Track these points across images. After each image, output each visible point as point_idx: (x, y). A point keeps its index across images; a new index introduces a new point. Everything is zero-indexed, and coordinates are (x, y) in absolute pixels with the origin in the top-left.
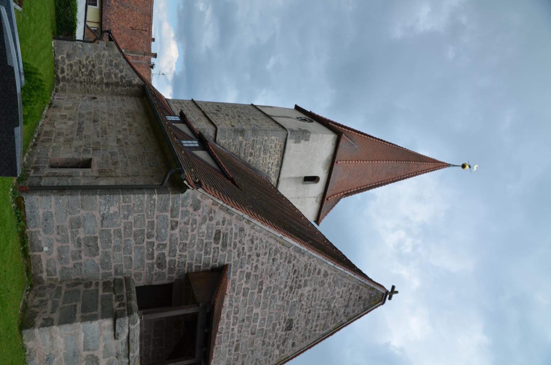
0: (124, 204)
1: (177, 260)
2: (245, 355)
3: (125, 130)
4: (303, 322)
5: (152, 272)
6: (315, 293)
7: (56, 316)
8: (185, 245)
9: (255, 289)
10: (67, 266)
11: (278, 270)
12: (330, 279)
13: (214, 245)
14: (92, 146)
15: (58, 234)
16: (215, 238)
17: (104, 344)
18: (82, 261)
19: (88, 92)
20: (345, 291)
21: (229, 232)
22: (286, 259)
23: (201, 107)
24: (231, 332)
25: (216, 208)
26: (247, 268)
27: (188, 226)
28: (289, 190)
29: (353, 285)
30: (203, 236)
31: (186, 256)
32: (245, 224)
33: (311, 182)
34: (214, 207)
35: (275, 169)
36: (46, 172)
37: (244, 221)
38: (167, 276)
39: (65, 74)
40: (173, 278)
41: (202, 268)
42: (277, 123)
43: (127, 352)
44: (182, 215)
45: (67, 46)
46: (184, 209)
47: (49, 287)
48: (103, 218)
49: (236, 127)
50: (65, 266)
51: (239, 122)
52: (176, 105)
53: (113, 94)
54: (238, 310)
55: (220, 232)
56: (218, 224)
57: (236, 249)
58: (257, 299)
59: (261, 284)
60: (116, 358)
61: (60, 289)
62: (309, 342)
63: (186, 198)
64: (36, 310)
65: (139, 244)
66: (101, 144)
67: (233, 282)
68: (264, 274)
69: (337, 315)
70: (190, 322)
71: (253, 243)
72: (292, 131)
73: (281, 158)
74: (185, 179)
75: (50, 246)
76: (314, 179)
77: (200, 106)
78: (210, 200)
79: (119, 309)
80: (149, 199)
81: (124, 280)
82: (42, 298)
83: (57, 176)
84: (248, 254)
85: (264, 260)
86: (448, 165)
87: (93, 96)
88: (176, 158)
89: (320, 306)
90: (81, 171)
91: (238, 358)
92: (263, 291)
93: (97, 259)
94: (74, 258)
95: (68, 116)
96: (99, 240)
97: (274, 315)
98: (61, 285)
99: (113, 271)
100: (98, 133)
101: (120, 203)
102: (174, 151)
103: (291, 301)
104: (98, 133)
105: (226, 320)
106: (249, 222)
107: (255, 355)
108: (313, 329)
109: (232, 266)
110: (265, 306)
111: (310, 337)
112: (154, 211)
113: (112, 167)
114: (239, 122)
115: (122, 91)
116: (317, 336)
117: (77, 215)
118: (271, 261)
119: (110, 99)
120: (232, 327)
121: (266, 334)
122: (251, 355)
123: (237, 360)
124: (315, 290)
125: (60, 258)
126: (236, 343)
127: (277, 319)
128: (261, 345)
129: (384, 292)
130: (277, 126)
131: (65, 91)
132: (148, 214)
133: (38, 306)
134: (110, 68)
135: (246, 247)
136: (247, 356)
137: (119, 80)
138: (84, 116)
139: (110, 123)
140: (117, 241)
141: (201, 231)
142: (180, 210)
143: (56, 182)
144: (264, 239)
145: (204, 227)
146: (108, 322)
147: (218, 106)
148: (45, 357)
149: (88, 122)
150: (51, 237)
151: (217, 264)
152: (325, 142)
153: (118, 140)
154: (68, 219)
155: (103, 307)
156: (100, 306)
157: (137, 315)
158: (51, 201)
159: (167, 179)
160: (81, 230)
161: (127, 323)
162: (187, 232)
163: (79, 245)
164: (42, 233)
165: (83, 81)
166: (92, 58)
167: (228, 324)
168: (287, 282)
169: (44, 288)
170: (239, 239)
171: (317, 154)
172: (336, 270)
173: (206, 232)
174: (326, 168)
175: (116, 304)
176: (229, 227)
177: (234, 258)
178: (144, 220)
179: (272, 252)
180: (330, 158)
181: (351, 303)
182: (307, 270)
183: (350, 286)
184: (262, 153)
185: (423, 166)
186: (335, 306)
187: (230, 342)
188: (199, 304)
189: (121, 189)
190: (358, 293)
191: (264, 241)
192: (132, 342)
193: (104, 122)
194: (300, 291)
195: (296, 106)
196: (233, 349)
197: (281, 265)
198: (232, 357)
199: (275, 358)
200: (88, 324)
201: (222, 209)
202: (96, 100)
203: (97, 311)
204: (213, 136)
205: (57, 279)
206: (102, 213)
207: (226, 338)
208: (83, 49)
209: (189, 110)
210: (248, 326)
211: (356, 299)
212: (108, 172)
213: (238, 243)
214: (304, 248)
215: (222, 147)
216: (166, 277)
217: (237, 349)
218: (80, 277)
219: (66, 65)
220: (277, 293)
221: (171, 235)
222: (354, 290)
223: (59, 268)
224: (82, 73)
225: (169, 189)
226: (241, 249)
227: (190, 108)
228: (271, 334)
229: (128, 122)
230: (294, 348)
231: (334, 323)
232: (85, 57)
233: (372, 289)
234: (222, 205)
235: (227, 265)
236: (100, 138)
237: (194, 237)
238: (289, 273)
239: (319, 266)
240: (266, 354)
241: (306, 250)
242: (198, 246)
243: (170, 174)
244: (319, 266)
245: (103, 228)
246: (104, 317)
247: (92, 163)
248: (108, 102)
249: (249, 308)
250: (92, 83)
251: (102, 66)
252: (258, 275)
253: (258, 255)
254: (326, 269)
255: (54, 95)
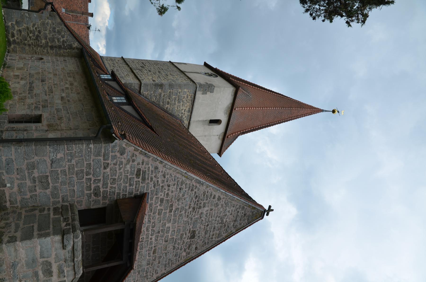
0: (68, 152)
1: (109, 190)
2: (161, 257)
3: (67, 88)
4: (203, 232)
5: (90, 200)
6: (211, 212)
7: (18, 234)
8: (114, 179)
9: (167, 210)
10: (26, 197)
11: (184, 196)
12: (222, 202)
13: (136, 179)
14: (41, 104)
15: (18, 174)
16: (136, 175)
17: (55, 253)
18: (37, 193)
19: (36, 53)
20: (233, 210)
21: (147, 169)
22: (189, 188)
23: (129, 64)
24: (150, 241)
25: (137, 153)
26: (161, 195)
27: (116, 166)
28: (198, 131)
29: (240, 206)
30: (128, 173)
31: (115, 188)
32: (159, 164)
33: (215, 124)
34: (136, 153)
35: (187, 114)
36: (5, 127)
37: (158, 162)
38: (101, 202)
39: (16, 38)
40: (106, 203)
41: (127, 196)
42: (189, 78)
43: (73, 258)
44: (112, 158)
45: (15, 14)
46: (113, 154)
47: (12, 213)
48: (52, 162)
49: (157, 82)
50: (24, 197)
51: (159, 77)
52: (109, 62)
53: (56, 55)
54: (155, 225)
55: (140, 170)
56: (138, 164)
57: (153, 182)
58: (169, 217)
59: (172, 206)
60: (64, 263)
61: (20, 214)
62: (207, 246)
63: (114, 146)
64: (3, 230)
65: (80, 179)
66: (49, 101)
67: (151, 205)
68: (173, 199)
69: (228, 227)
70: (119, 234)
71: (165, 177)
72: (201, 85)
73: (191, 106)
74: (114, 133)
75: (12, 183)
76: (217, 122)
77: (128, 63)
78: (132, 147)
79: (66, 228)
80: (87, 148)
81: (69, 206)
82: (7, 221)
83: (15, 130)
84: (161, 185)
85: (173, 189)
86: (322, 111)
87: (40, 56)
88: (107, 116)
89: (215, 221)
90: (33, 126)
91: (155, 259)
92: (173, 211)
93: (48, 191)
94: (31, 191)
95: (20, 76)
96: (49, 178)
97: (181, 228)
98: (21, 211)
99: (60, 199)
100: (46, 92)
101: (64, 151)
102: (105, 108)
103: (194, 218)
104: (46, 92)
105: (146, 232)
106: (161, 162)
107: (168, 256)
108: (211, 237)
109: (150, 194)
110: (175, 221)
111: (208, 243)
112: (91, 156)
113: (58, 122)
114: (159, 77)
115: (64, 53)
116: (214, 242)
117: (32, 160)
118: (178, 190)
119: (55, 60)
120: (150, 237)
121: (176, 241)
122: (165, 257)
123: (155, 260)
124: (211, 210)
125: (20, 192)
126: (153, 248)
127: (183, 231)
128: (172, 250)
129: (263, 210)
130: (189, 81)
131: (16, 52)
132: (86, 158)
133: (4, 228)
134: (54, 34)
135: (160, 180)
136: (162, 257)
137: (61, 44)
138: (33, 76)
139: (55, 82)
140: (64, 178)
141: (126, 169)
142: (110, 155)
143: (14, 135)
144: (173, 174)
145: (128, 167)
146: (58, 238)
147: (143, 63)
148: (11, 264)
149: (37, 81)
150: (12, 176)
151: (139, 193)
152: (224, 94)
153: (62, 98)
154: (25, 164)
155: (54, 227)
156: (51, 226)
157: (79, 232)
158: (11, 151)
159: (100, 132)
160: (35, 171)
161: (72, 238)
162: (116, 171)
163: (34, 181)
164: (5, 174)
165: (31, 44)
166: (38, 25)
167: (147, 235)
168: (190, 204)
169: (8, 214)
170: (154, 175)
171: (220, 103)
172: (227, 195)
173: (130, 170)
174: (226, 113)
175: (63, 224)
176: (147, 166)
177: (151, 188)
178: (83, 162)
179: (179, 184)
180: (230, 106)
181: (238, 219)
182: (205, 196)
183: (238, 207)
184: (177, 102)
185: (302, 112)
186: (226, 221)
187: (149, 248)
188: (124, 223)
189: (66, 140)
190: (243, 211)
191: (173, 176)
192: (76, 250)
193: (50, 81)
194: (200, 211)
195: (205, 63)
196: (152, 252)
197: (186, 192)
198: (151, 258)
199: (182, 258)
200: (43, 240)
201: (142, 154)
202: (43, 60)
203: (49, 229)
204: (138, 89)
205: (18, 206)
206: (51, 158)
207: (146, 245)
208: (30, 18)
209: (119, 67)
210: (162, 236)
211: (242, 215)
212: (55, 127)
213: (154, 177)
214: (202, 180)
215: (146, 97)
216: (101, 203)
217: (154, 252)
218: (35, 204)
219: (16, 30)
220: (183, 212)
221: (104, 173)
222: (241, 209)
223: (19, 198)
224: (30, 37)
225: (102, 139)
226: (156, 181)
227: (121, 65)
228: (179, 241)
229: (70, 81)
230: (197, 251)
231: (226, 232)
232: (32, 24)
233: (254, 208)
234: (141, 151)
235: (146, 193)
236: (48, 96)
237: (121, 173)
238: (192, 198)
239: (214, 193)
240: (176, 256)
241: (204, 181)
242: (124, 180)
243: (103, 130)
244: (214, 193)
245: (52, 169)
246: (55, 234)
247: (42, 119)
248: (53, 62)
249: (162, 224)
250: (39, 46)
251: (47, 32)
252: (169, 200)
253: (169, 186)
254: (220, 195)
255: (7, 55)
